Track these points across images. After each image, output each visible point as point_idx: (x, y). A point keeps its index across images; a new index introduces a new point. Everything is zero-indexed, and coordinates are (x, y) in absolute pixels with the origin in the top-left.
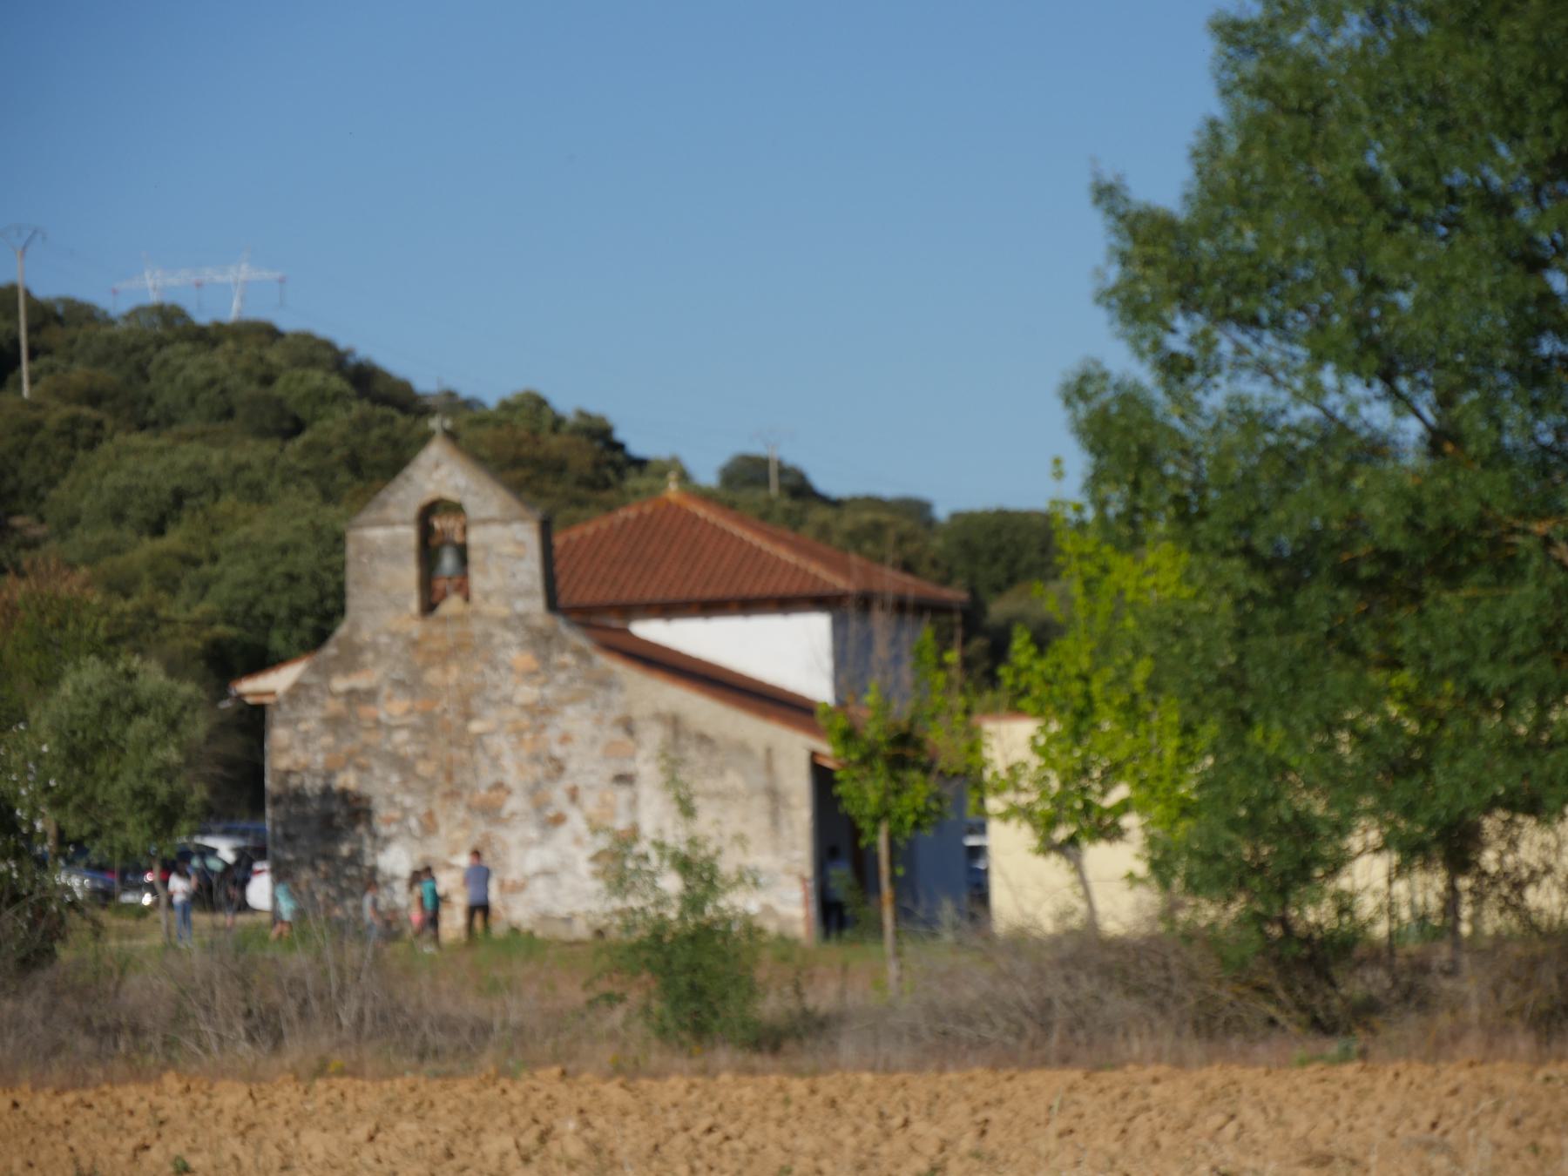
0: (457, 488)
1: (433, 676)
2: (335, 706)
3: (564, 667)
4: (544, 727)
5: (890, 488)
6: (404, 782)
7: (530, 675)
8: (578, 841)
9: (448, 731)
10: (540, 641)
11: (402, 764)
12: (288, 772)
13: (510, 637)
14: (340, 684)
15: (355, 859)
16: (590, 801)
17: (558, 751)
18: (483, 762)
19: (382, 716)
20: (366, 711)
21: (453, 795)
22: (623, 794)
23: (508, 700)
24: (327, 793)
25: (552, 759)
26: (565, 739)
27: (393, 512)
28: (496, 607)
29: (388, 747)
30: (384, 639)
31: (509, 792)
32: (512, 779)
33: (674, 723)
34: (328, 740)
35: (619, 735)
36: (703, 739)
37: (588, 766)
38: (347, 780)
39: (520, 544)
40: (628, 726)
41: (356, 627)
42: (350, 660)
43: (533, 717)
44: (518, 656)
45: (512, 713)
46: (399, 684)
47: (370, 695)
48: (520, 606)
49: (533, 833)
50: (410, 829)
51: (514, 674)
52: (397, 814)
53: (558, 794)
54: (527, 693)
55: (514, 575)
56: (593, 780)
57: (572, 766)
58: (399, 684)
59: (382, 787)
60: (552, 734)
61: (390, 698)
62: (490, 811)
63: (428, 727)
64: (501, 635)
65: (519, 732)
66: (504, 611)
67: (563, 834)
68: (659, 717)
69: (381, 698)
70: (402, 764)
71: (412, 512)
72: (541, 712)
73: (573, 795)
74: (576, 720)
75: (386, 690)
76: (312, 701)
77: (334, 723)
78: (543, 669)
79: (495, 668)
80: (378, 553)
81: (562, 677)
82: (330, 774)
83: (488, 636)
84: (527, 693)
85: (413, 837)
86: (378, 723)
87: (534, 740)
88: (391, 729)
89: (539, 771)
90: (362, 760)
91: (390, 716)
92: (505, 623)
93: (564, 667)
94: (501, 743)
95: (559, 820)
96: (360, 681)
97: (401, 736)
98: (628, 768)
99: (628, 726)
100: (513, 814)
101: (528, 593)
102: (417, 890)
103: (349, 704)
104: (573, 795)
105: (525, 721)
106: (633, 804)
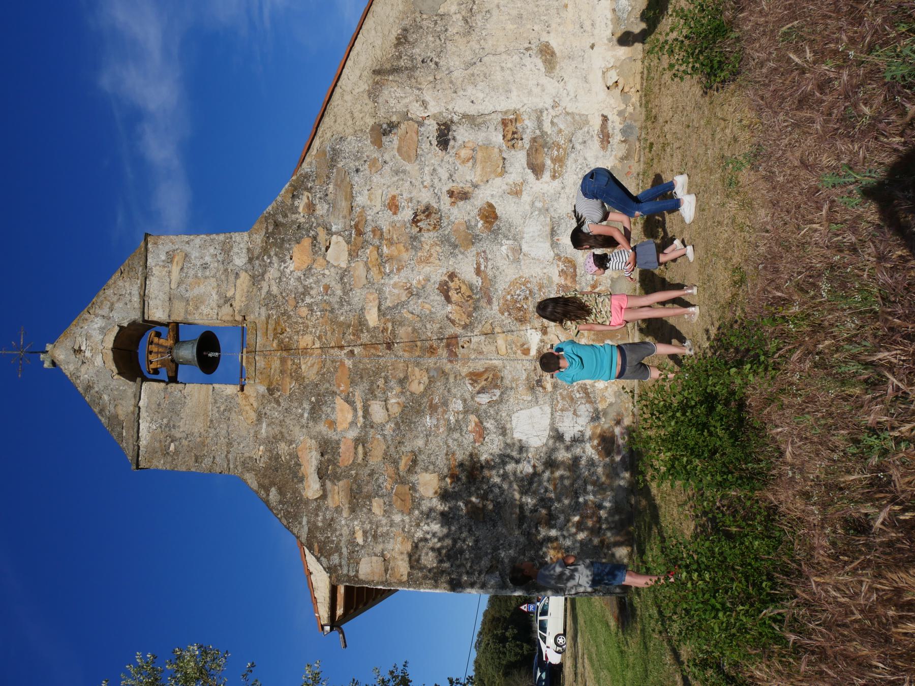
0: (103, 331)
1: (309, 368)
2: (338, 496)
3: (311, 207)
4: (377, 231)
5: (481, 618)
6: (433, 408)
7: (319, 249)
8: (516, 192)
9: (376, 349)
10: (280, 235)
11: (408, 416)
12: (414, 559)
13: (272, 273)
14: (312, 488)
15: (529, 483)
16: (467, 175)
17: (407, 214)
18: (416, 306)
19: (352, 434)
20: (346, 455)
21: (451, 343)
22: (462, 134)
23: (343, 275)
24: (446, 518)
25: (415, 221)
26: (393, 206)
27: (124, 410)
28: (240, 288)
29: (389, 428)
30: (264, 430)
31: (452, 276)
32: (438, 274)
33: (382, 73)
34: (377, 506)
35: (393, 141)
36: (402, 40)
37: (426, 178)
38: (428, 484)
39: (170, 259)
40: (383, 131)
41: (248, 464)
42: (282, 473)
43: (365, 244)
44: (298, 258)
45: (359, 270)
46: (315, 412)
47: (327, 448)
48: (240, 260)
49: (505, 248)
50: (490, 404)
51: (323, 268)
52: (473, 418)
53: (460, 214)
54: (338, 252)
55: (205, 267)
56: (443, 173)
57: (426, 197)
58: (315, 412)
59: (442, 442)
60: (385, 220)
61: (332, 424)
62: (476, 298)
63: (370, 380)
64: (269, 283)
65: (382, 261)
66: (244, 278)
67: (507, 209)
68: (373, 93)
69: (332, 435)
70: (408, 416)
71: (127, 386)
72: (359, 234)
73: (460, 196)
74: (370, 196)
75: (322, 428)
76: (330, 524)
77: (358, 499)
78: (313, 235)
79: (306, 291)
80: (167, 432)
81: (321, 209)
82: (605, 44)
83: (270, 300)
84: (338, 252)
85: (501, 401)
86: (360, 441)
87: (391, 242)
88: (369, 424)
89: (428, 238)
90: (403, 464)
91: (353, 423)
92: (256, 279)
93: (311, 207)
94: (392, 288)
95: (490, 215)
96: (310, 462)
97: (378, 412)
98: (431, 128)
99: (383, 131)
100: (478, 272)
101: (226, 250)
102: (668, 360)
103: (336, 478)
104: (460, 196)
105: (369, 252)
106: (472, 120)
